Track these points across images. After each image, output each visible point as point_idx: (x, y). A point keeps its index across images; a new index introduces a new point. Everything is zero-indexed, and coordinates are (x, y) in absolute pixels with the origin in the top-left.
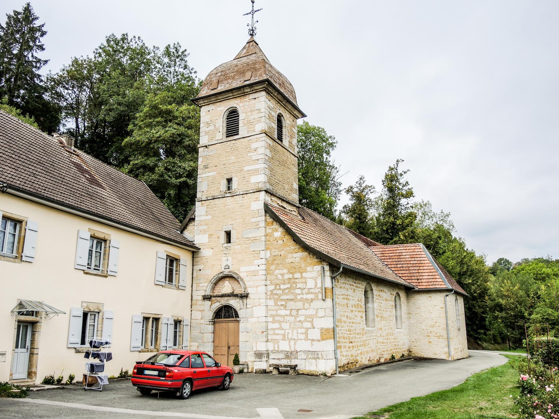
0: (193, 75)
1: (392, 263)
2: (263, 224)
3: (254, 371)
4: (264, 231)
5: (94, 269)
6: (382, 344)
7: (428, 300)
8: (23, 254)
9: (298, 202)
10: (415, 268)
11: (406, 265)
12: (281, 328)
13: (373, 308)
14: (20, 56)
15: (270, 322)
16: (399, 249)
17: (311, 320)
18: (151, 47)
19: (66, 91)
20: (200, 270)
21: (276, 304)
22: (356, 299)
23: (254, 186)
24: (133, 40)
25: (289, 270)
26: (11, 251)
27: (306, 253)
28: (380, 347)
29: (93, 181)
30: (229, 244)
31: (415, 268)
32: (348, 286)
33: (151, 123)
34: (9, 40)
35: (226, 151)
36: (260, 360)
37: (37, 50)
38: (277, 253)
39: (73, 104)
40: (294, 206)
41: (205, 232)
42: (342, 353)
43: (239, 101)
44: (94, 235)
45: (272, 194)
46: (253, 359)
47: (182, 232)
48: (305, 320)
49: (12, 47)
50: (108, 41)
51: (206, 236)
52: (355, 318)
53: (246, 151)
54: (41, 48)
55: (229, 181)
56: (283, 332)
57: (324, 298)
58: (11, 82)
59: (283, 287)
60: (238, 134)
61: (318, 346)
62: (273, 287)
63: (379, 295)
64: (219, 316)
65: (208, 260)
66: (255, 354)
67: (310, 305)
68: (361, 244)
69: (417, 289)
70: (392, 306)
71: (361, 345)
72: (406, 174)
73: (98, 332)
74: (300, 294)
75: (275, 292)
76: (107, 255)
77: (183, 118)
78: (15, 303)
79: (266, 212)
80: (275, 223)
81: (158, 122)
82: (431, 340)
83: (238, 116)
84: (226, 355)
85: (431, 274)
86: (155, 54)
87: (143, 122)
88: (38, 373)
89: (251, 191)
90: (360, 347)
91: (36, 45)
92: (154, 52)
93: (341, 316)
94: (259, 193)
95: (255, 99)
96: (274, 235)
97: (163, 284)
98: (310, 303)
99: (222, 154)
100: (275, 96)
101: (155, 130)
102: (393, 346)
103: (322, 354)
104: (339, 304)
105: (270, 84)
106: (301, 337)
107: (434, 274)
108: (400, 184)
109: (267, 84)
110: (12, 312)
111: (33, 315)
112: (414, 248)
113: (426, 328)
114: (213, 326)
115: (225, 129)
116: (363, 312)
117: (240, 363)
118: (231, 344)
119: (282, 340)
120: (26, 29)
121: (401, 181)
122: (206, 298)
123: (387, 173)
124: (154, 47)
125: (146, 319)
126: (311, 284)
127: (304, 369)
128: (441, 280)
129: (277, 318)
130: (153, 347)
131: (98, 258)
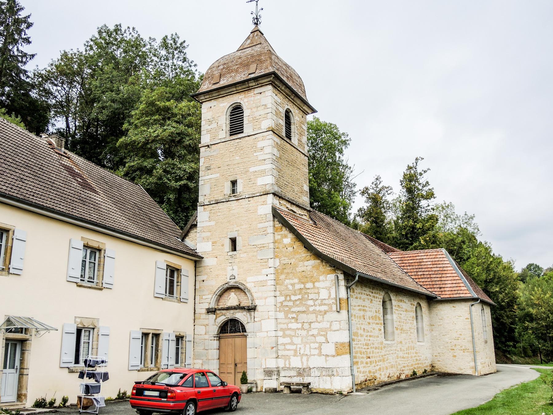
0: (193, 69)
1: (412, 270)
2: (271, 230)
3: (264, 390)
4: (272, 238)
5: (88, 281)
8: (11, 266)
11: (427, 273)
12: (292, 343)
15: (281, 337)
16: (420, 255)
17: (325, 333)
18: (146, 39)
19: (55, 88)
20: (203, 281)
22: (374, 310)
23: (261, 188)
24: (127, 32)
25: (300, 279)
28: (401, 362)
29: (86, 185)
33: (148, 121)
35: (230, 151)
36: (270, 378)
39: (62, 101)
40: (305, 209)
41: (208, 239)
42: (359, 370)
43: (244, 96)
44: (87, 244)
46: (262, 377)
47: (183, 240)
48: (319, 334)
54: (27, 41)
55: (234, 183)
56: (294, 347)
59: (293, 298)
60: (243, 132)
61: (332, 363)
62: (283, 298)
63: (399, 306)
64: (225, 331)
65: (211, 270)
66: (264, 371)
69: (439, 298)
70: (413, 317)
73: (94, 349)
75: (285, 304)
76: (102, 266)
77: (182, 115)
80: (284, 229)
81: (155, 120)
83: (243, 113)
85: (455, 282)
86: (151, 46)
88: (28, 395)
91: (21, 38)
92: (150, 43)
95: (261, 93)
96: (283, 241)
97: (164, 297)
98: (323, 315)
100: (282, 90)
101: (152, 129)
103: (337, 371)
105: (277, 77)
107: (458, 281)
108: (420, 184)
109: (273, 78)
111: (22, 333)
112: (436, 253)
113: (450, 341)
115: (229, 126)
116: (381, 324)
117: (248, 381)
119: (294, 356)
120: (10, 21)
122: (211, 311)
124: (150, 38)
126: (324, 294)
129: (288, 332)
130: (153, 365)
131: (92, 269)
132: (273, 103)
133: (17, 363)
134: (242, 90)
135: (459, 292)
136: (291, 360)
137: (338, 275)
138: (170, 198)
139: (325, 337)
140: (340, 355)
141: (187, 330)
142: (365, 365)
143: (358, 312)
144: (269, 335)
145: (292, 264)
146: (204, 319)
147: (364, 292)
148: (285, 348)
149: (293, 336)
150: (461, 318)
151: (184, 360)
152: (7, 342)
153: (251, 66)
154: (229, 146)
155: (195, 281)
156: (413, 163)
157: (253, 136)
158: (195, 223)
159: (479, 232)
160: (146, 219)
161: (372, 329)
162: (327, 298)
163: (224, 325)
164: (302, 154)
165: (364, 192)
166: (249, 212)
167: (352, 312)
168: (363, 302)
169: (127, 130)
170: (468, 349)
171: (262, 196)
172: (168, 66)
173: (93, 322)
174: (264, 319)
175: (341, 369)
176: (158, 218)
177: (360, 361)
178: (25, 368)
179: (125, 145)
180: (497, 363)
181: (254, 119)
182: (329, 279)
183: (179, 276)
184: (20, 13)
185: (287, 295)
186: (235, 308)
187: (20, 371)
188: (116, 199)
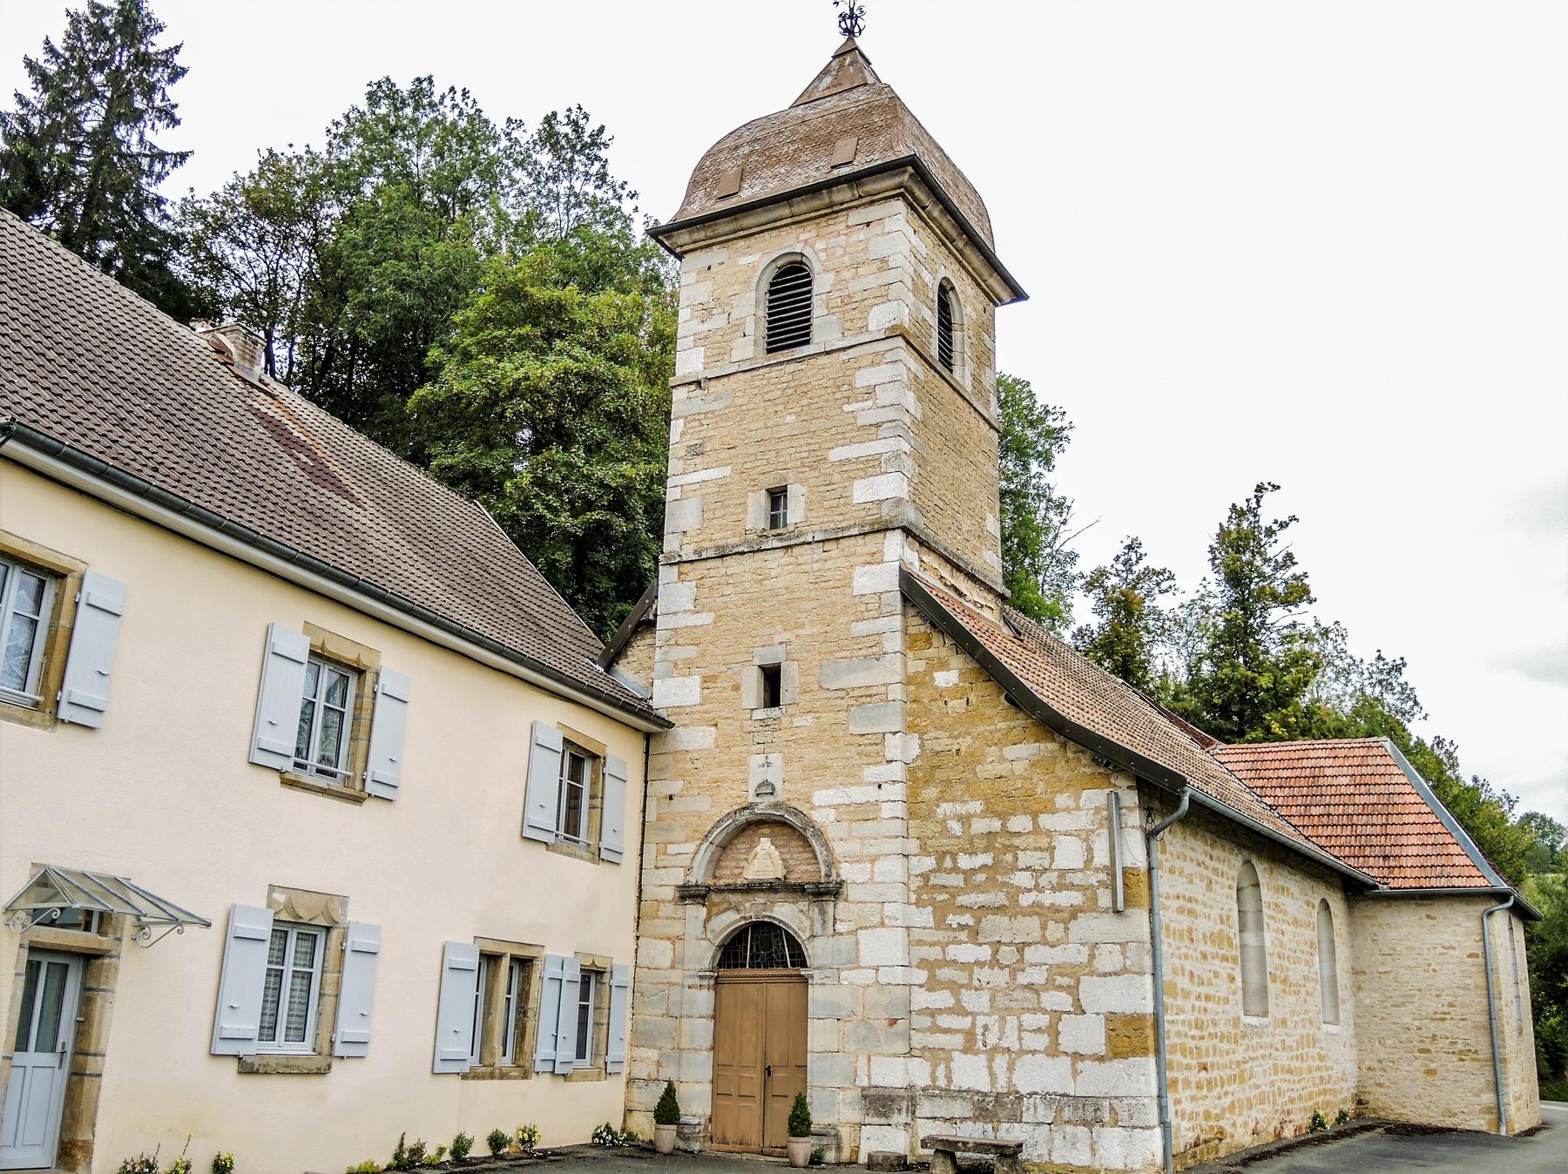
0: (627, 206)
1: (1290, 801)
2: (894, 643)
3: (863, 1159)
4: (899, 668)
5: (319, 771)
6: (1288, 1077)
7: (1422, 926)
8: (63, 697)
9: (1000, 580)
10: (1375, 819)
11: (1340, 810)
12: (958, 1010)
13: (1262, 949)
14: (103, 139)
15: (921, 986)
16: (1312, 754)
17: (1072, 982)
18: (499, 124)
19: (239, 253)
20: (671, 798)
21: (940, 924)
22: (1215, 913)
23: (863, 513)
24: (448, 102)
25: (987, 802)
26: (17, 682)
27: (1053, 746)
28: (1284, 1086)
29: (320, 475)
30: (775, 712)
31: (1375, 819)
32: (1190, 868)
33: (502, 340)
34: (73, 89)
35: (767, 397)
36: (883, 1121)
37: (157, 122)
38: (944, 742)
39: (257, 292)
40: (990, 590)
41: (688, 667)
42: (1179, 1107)
43: (814, 233)
44: (323, 647)
45: (922, 543)
46: (855, 1115)
47: (609, 668)
48: (1050, 984)
49: (81, 112)
50: (373, 99)
51: (695, 682)
52: (1214, 981)
53: (838, 395)
54: (169, 116)
55: (777, 496)
56: (965, 1023)
57: (1120, 906)
58: (74, 214)
59: (965, 862)
60: (807, 342)
61: (1097, 1080)
62: (929, 863)
63: (1277, 905)
64: (736, 959)
65: (698, 764)
66: (865, 1097)
67: (1066, 929)
68: (1184, 739)
69: (1384, 889)
70: (1312, 943)
71: (1232, 1079)
72: (1285, 531)
73: (325, 998)
74: (1029, 890)
75: (936, 880)
76: (365, 722)
77: (601, 329)
78: (20, 879)
79: (905, 599)
80: (937, 640)
81: (520, 338)
82: (1433, 1066)
83: (809, 283)
84: (759, 1097)
85: (1431, 840)
86: (510, 140)
87: (474, 339)
88: (96, 1147)
89: (855, 531)
90: (1229, 1084)
91: (153, 108)
92: (508, 134)
93: (1175, 972)
94: (881, 535)
95: (868, 224)
96: (933, 680)
97: (550, 839)
98: (1066, 922)
99: (749, 406)
100: (934, 219)
101: (511, 361)
102: (1317, 1081)
103: (1112, 1109)
104: (1167, 928)
105: (922, 176)
106: (1032, 1042)
107: (1440, 839)
108: (1266, 561)
109: (911, 176)
110: (10, 910)
111: (87, 928)
112: (1363, 752)
113: (1417, 1023)
114: (712, 992)
115: (764, 325)
116: (1234, 960)
117: (813, 1128)
118: (776, 1057)
119: (965, 1051)
120: (123, 58)
121: (1271, 552)
122: (690, 894)
123: (1225, 525)
124: (509, 120)
125: (490, 959)
126: (1069, 854)
127: (1046, 1158)
128: (1468, 862)
129: (944, 974)
130: (507, 1061)
131: (334, 732)
132: (907, 254)
133: (66, 1034)
134: (808, 216)
135: (1447, 871)
136: (953, 1065)
137: (1119, 791)
138: (556, 560)
139: (1071, 994)
140: (1125, 1056)
141: (617, 951)
142: (1195, 1091)
143: (1175, 916)
144: (883, 980)
145: (962, 753)
146: (668, 918)
147: (1191, 854)
148: (934, 1023)
149: (962, 986)
150: (1456, 953)
151: (603, 1046)
152: (36, 958)
153: (839, 143)
154: (765, 382)
155: (645, 796)
156: (1248, 500)
157: (841, 354)
158: (651, 617)
159: (1416, 708)
160: (501, 597)
161: (1211, 975)
162: (1081, 866)
163: (733, 940)
164: (982, 422)
165: (1095, 582)
166: (823, 585)
167: (1165, 916)
168: (1189, 886)
169: (439, 367)
170: (1476, 1052)
171: (868, 538)
172: (557, 198)
173: (326, 906)
174: (866, 928)
175: (1125, 1101)
176: (534, 601)
177: (1181, 1077)
178: (92, 1050)
179: (430, 409)
180: (1543, 1097)
181: (847, 300)
182: (1088, 805)
183: (597, 777)
184: (153, 39)
185: (944, 853)
186: (771, 888)
187: (73, 1062)
188: (414, 528)
